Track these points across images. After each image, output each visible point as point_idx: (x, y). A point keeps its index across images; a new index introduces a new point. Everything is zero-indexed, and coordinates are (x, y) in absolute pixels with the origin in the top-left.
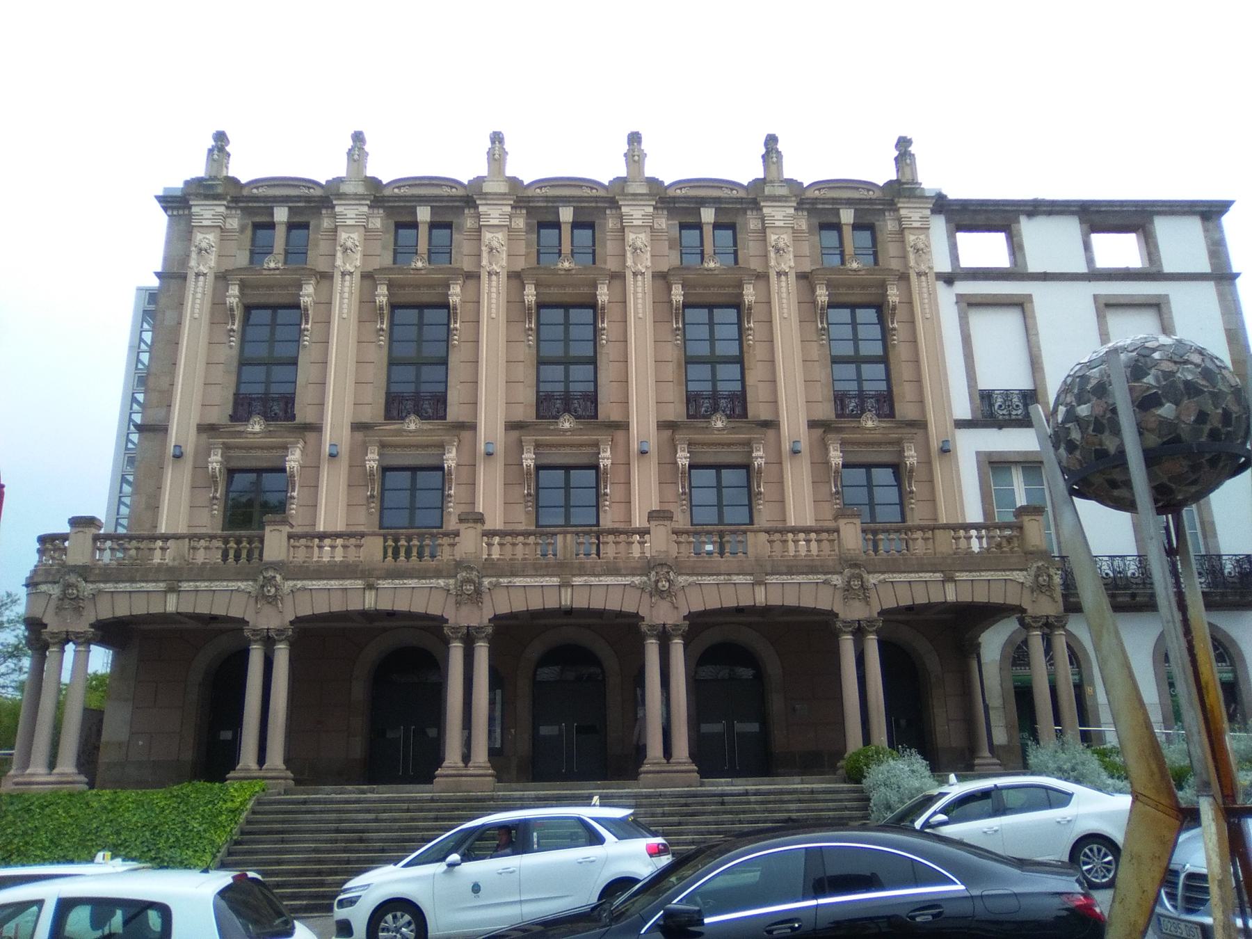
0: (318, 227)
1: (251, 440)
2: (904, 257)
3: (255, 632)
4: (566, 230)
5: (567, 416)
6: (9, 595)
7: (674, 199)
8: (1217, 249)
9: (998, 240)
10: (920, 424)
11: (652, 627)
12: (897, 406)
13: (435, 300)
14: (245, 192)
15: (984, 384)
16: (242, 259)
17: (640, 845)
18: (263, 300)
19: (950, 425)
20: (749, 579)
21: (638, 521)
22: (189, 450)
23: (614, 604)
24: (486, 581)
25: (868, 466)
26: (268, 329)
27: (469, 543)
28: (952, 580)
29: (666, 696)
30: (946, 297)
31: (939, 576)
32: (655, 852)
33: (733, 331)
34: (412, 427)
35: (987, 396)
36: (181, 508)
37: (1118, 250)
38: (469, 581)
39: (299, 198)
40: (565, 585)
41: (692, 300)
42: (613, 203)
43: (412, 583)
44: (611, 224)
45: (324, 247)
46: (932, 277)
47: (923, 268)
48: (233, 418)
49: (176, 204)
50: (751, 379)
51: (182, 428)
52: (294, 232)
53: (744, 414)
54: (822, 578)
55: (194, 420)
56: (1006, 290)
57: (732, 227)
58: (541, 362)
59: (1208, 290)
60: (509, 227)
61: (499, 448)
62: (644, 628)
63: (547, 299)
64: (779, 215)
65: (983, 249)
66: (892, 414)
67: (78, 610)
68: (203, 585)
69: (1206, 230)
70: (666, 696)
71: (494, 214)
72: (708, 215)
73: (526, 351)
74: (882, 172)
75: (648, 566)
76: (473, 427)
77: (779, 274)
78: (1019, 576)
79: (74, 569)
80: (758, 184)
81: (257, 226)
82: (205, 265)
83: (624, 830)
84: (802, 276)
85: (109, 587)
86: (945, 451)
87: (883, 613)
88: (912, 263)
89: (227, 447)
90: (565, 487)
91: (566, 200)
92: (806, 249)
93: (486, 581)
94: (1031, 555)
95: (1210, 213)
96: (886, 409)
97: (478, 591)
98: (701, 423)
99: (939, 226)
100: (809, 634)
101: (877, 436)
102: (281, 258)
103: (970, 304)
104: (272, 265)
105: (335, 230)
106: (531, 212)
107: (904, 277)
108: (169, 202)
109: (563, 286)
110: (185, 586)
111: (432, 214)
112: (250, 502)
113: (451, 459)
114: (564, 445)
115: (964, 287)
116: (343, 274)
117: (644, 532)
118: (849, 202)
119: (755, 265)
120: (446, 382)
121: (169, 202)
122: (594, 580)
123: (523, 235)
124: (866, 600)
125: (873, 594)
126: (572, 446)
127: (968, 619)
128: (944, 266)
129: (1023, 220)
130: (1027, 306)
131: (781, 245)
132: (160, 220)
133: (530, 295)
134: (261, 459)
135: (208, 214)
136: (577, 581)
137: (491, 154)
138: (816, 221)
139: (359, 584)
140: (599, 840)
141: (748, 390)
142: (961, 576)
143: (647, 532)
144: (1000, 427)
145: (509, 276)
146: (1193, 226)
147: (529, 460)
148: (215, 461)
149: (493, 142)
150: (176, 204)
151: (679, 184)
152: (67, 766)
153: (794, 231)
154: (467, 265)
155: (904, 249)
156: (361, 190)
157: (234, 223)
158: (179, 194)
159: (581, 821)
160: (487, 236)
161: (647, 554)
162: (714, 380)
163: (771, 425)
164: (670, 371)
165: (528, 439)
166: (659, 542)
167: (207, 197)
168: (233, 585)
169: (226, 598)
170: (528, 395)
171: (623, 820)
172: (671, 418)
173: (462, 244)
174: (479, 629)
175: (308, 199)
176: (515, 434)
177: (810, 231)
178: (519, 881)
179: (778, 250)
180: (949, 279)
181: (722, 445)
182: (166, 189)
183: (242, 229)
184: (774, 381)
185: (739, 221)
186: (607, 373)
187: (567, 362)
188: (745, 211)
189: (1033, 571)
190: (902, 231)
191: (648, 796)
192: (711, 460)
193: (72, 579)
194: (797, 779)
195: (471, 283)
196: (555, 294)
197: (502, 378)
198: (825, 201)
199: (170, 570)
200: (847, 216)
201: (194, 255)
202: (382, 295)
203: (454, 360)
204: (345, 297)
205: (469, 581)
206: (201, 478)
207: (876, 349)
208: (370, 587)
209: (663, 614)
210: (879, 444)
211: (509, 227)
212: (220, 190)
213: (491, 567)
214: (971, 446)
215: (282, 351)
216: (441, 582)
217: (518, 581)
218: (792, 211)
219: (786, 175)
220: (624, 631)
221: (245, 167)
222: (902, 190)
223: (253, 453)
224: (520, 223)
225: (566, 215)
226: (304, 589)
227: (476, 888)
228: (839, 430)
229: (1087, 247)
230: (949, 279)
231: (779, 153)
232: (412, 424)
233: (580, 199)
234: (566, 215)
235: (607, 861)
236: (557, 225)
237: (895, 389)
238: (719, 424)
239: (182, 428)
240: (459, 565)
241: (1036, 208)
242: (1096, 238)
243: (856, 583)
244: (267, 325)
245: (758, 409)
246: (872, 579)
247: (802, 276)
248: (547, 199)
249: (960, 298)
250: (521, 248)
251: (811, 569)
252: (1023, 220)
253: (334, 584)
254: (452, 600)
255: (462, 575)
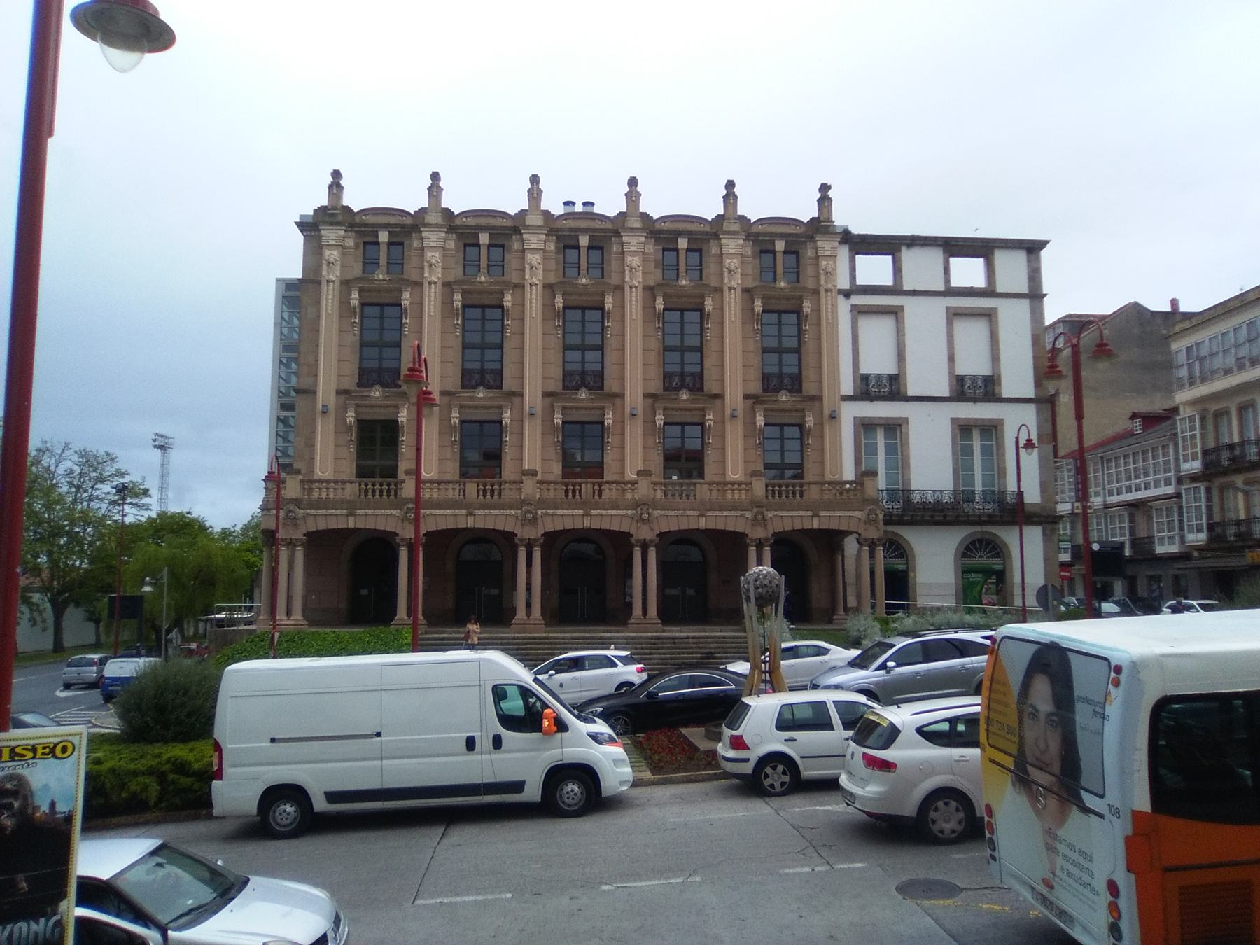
0: (410, 246)
1: (374, 402)
2: (817, 277)
3: (403, 540)
4: (583, 252)
5: (584, 389)
6: (108, 454)
7: (660, 232)
8: (1034, 276)
9: (979, 263)
10: (818, 398)
11: (638, 541)
12: (804, 385)
13: (494, 303)
14: (357, 219)
15: (864, 370)
16: (357, 270)
17: (633, 668)
18: (374, 301)
19: (838, 398)
20: (696, 513)
21: (631, 475)
22: (332, 407)
23: (615, 527)
24: (539, 512)
25: (782, 426)
26: (479, 322)
27: (529, 488)
28: (817, 515)
29: (645, 579)
30: (844, 307)
31: (809, 513)
32: (640, 671)
33: (794, 331)
34: (481, 395)
35: (865, 378)
36: (331, 457)
37: (968, 272)
38: (530, 512)
39: (396, 225)
40: (587, 514)
41: (669, 306)
42: (617, 233)
43: (496, 512)
44: (615, 248)
45: (415, 262)
46: (835, 292)
47: (830, 286)
48: (359, 385)
49: (309, 227)
50: (707, 364)
51: (326, 393)
52: (392, 247)
53: (701, 389)
54: (739, 513)
55: (334, 387)
56: (885, 304)
57: (797, 253)
58: (566, 348)
59: (1025, 304)
60: (544, 251)
61: (538, 410)
62: (633, 540)
63: (570, 304)
64: (732, 244)
65: (875, 270)
66: (800, 391)
67: (296, 525)
68: (370, 512)
69: (1029, 261)
70: (645, 579)
71: (534, 240)
72: (683, 243)
73: (555, 341)
74: (806, 211)
75: (636, 505)
76: (521, 395)
77: (730, 289)
78: (858, 514)
79: (291, 501)
80: (719, 219)
81: (365, 243)
82: (332, 275)
83: (626, 661)
84: (746, 291)
85: (313, 512)
86: (834, 417)
87: (774, 534)
88: (822, 283)
89: (357, 406)
90: (582, 451)
91: (584, 231)
92: (749, 270)
93: (539, 512)
94: (867, 501)
95: (1033, 248)
96: (797, 387)
97: (535, 518)
98: (672, 395)
99: (844, 252)
100: (729, 548)
101: (788, 406)
102: (385, 269)
103: (858, 311)
104: (381, 277)
105: (422, 249)
106: (559, 238)
107: (816, 292)
108: (303, 225)
109: (581, 295)
110: (359, 512)
111: (490, 238)
112: (377, 444)
113: (507, 418)
114: (581, 408)
115: (858, 300)
116: (730, 289)
117: (634, 483)
118: (782, 236)
119: (714, 283)
120: (502, 361)
121: (303, 225)
122: (604, 512)
123: (553, 256)
124: (765, 527)
125: (769, 523)
126: (586, 409)
127: (831, 540)
128: (844, 284)
129: (904, 249)
130: (900, 314)
131: (733, 267)
132: (298, 238)
133: (559, 302)
134: (381, 414)
135: (333, 236)
136: (594, 512)
137: (725, 198)
138: (758, 249)
139: (464, 512)
140: (615, 665)
141: (706, 372)
142: (822, 513)
143: (636, 483)
144: (872, 401)
145: (544, 287)
146: (1021, 257)
147: (558, 419)
148: (351, 416)
149: (532, 183)
150: (309, 227)
151: (664, 219)
152: (297, 616)
153: (444, 249)
154: (515, 279)
155: (818, 272)
156: (440, 221)
157: (350, 242)
158: (311, 220)
159: (607, 657)
160: (529, 256)
161: (633, 492)
162: (682, 363)
163: (720, 396)
164: (653, 358)
165: (558, 405)
166: (644, 490)
167: (331, 224)
168: (388, 512)
169: (381, 518)
170: (556, 372)
171: (915, 785)
172: (653, 391)
173: (511, 262)
174: (535, 540)
175: (403, 226)
176: (549, 400)
177: (754, 257)
178: (580, 682)
179: (730, 271)
180: (847, 294)
181: (685, 410)
182: (302, 216)
183: (357, 246)
184: (722, 366)
185: (705, 248)
186: (611, 358)
187: (583, 348)
188: (708, 241)
189: (866, 511)
190: (817, 257)
191: (633, 638)
192: (678, 420)
193: (292, 507)
194: (718, 628)
195: (518, 291)
196: (575, 300)
197: (540, 360)
198: (765, 234)
199: (349, 502)
200: (780, 246)
201: (325, 267)
202: (458, 300)
203: (507, 346)
204: (432, 300)
205: (530, 512)
206: (341, 427)
207: (792, 343)
208: (471, 514)
209: (645, 533)
210: (789, 411)
211: (544, 251)
212: (340, 218)
213: (543, 503)
214: (851, 412)
215: (389, 336)
216: (513, 512)
217: (559, 512)
218: (741, 242)
219: (543, 207)
220: (621, 541)
221: (355, 199)
222: (820, 225)
223: (375, 410)
224: (551, 246)
225: (584, 241)
226: (431, 515)
227: (561, 685)
228: (763, 402)
229: (947, 270)
230: (847, 294)
231: (736, 197)
232: (481, 393)
233: (594, 230)
234: (584, 241)
235: (619, 674)
236: (578, 247)
237: (804, 373)
238: (685, 397)
239: (326, 393)
240: (523, 502)
241: (914, 242)
242: (954, 261)
243: (760, 517)
244: (379, 316)
245: (710, 386)
246: (770, 514)
247: (746, 291)
248: (571, 230)
249: (854, 307)
250: (552, 265)
251: (734, 508)
252: (904, 249)
253: (449, 512)
254: (519, 523)
255: (525, 508)
